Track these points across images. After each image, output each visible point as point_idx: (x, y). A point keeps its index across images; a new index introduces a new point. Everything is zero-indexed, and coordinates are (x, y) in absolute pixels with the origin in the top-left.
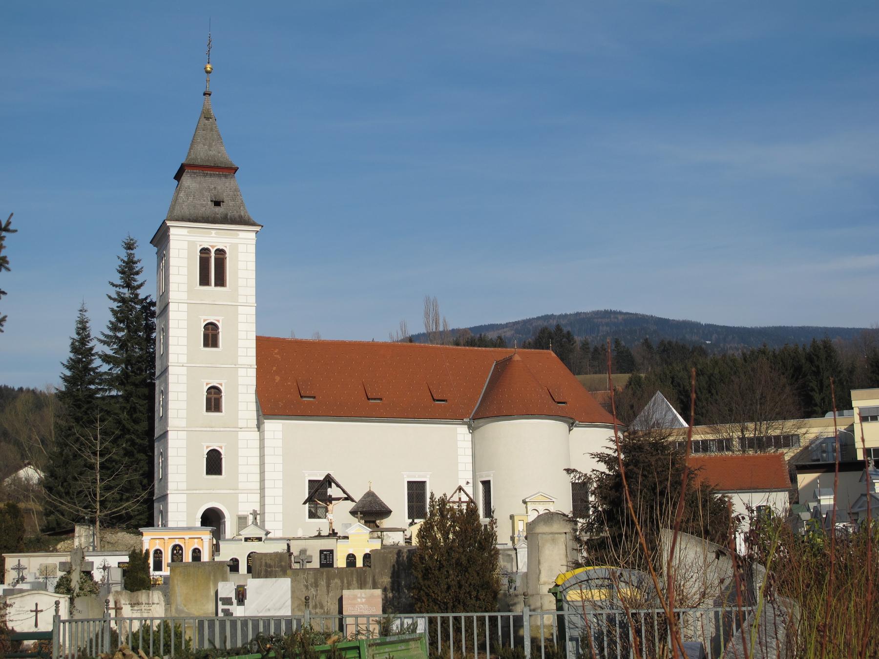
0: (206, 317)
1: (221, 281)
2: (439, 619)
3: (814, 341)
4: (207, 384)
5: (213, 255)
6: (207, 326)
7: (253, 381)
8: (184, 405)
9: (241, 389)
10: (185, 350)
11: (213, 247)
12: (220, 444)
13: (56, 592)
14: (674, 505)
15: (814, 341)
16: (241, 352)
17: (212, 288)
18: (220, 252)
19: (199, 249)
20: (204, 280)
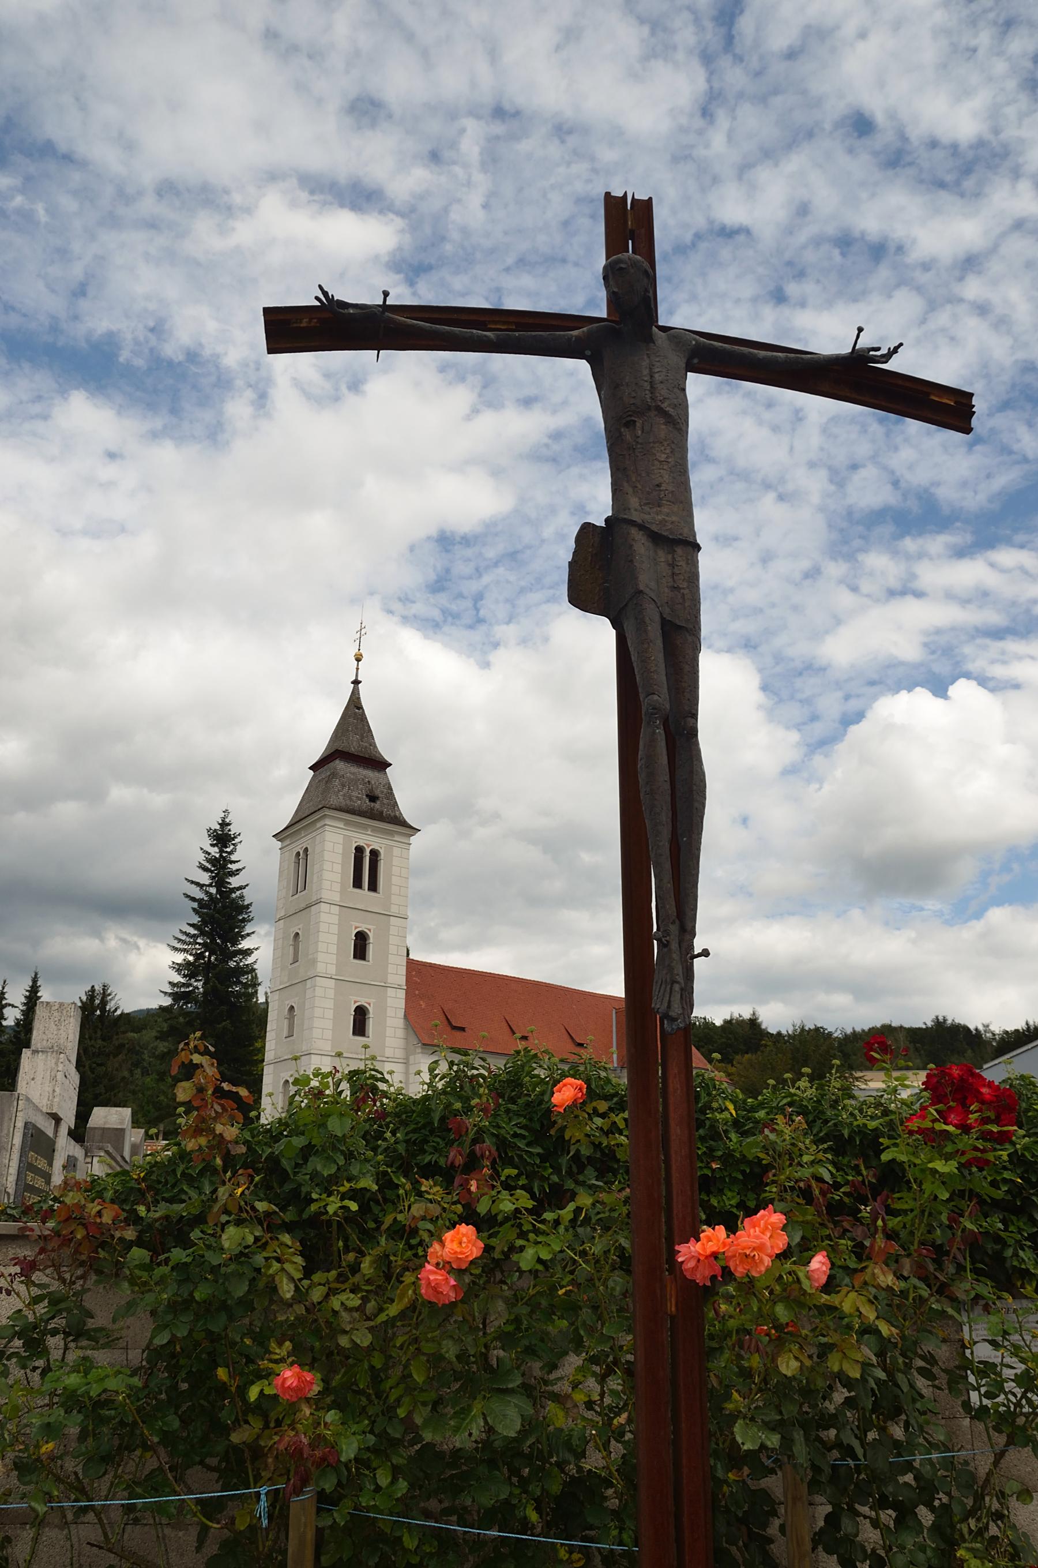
0: (357, 924)
1: (373, 887)
2: (252, 1485)
3: (937, 1017)
4: (355, 1002)
5: (367, 853)
6: (356, 848)
7: (402, 1004)
8: (329, 1024)
9: (390, 1012)
10: (333, 959)
11: (368, 846)
12: (367, 1000)
13: (26, 1123)
14: (158, 1537)
15: (937, 1017)
16: (391, 969)
17: (365, 892)
18: (375, 854)
19: (354, 846)
20: (357, 883)
